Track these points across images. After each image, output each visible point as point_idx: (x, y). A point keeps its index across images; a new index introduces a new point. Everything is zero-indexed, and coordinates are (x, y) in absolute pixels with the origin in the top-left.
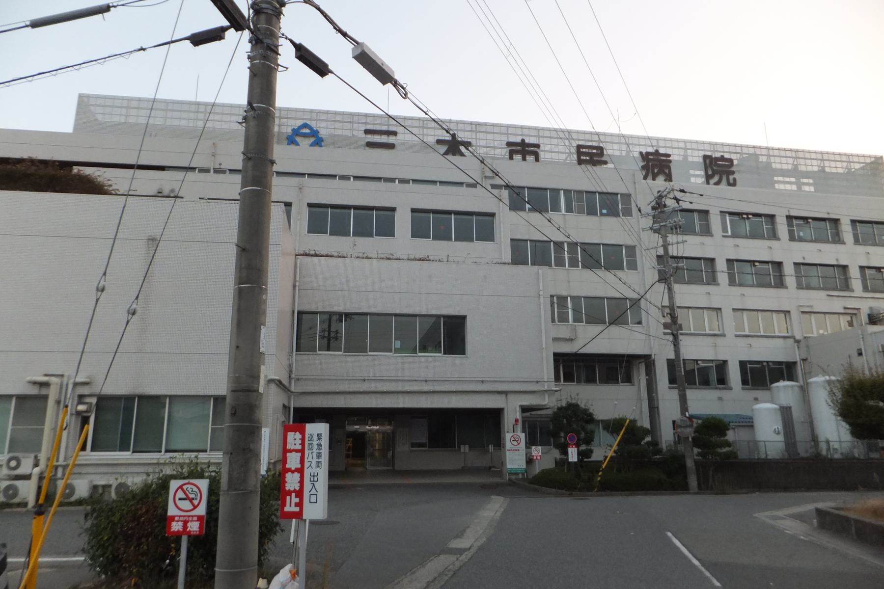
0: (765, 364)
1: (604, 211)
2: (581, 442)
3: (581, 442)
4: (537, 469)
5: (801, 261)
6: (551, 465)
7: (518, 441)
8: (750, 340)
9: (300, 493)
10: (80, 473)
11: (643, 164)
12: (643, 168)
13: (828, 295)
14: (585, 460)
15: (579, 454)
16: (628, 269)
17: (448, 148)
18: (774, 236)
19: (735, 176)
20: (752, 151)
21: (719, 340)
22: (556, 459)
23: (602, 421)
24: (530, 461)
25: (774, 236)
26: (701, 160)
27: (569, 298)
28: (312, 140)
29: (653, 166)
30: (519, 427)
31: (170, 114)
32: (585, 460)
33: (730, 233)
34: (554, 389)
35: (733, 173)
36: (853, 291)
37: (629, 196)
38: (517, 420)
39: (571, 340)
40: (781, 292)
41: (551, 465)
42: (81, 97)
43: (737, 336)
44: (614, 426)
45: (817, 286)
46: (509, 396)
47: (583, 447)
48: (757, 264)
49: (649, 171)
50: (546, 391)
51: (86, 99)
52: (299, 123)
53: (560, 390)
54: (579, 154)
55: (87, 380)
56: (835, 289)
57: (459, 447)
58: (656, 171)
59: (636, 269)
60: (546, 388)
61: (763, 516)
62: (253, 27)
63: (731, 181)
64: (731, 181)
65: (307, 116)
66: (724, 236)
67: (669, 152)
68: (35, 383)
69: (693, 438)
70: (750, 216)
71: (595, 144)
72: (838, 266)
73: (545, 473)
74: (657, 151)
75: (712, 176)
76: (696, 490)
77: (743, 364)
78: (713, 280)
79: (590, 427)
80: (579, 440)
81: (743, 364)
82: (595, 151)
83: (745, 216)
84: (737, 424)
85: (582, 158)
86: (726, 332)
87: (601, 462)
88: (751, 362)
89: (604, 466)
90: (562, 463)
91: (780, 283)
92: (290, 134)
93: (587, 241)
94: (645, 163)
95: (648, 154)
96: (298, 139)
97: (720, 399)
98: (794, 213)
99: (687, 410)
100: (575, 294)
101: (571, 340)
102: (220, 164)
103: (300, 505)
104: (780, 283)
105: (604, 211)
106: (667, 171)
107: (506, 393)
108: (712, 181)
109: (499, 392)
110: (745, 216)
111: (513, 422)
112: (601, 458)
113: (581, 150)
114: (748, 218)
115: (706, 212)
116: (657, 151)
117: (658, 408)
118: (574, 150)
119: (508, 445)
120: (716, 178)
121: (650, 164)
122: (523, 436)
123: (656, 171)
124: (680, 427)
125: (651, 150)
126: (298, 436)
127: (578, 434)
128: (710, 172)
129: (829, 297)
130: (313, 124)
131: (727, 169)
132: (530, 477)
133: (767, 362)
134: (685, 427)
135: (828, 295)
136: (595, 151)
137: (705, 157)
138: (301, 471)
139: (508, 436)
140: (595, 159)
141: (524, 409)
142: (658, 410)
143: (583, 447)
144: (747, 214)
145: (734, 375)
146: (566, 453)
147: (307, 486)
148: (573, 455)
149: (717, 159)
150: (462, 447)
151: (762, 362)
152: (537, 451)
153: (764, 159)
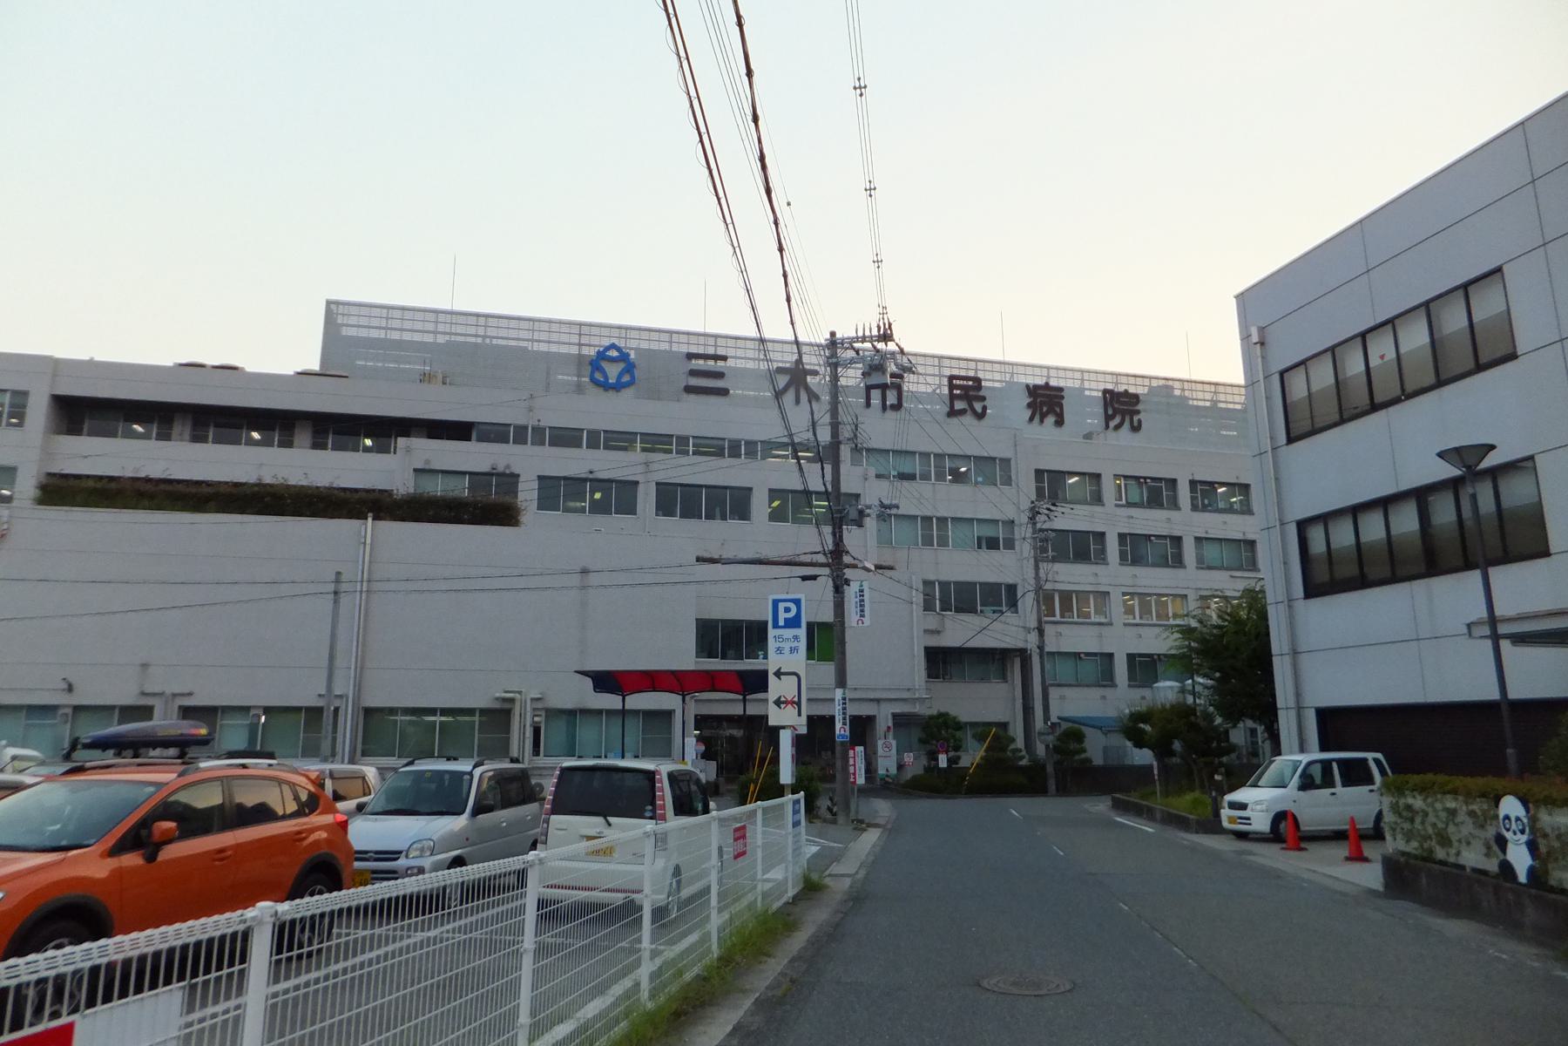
0: (1156, 657)
1: (980, 479)
2: (950, 749)
3: (950, 749)
4: (909, 774)
5: (1204, 535)
6: (921, 772)
7: (888, 747)
8: (1141, 630)
9: (854, 774)
10: (540, 775)
11: (1029, 400)
12: (1029, 406)
13: (1232, 577)
14: (954, 766)
15: (949, 760)
16: (1004, 549)
17: (790, 380)
18: (1174, 505)
19: (1141, 416)
20: (1162, 383)
21: (1105, 630)
22: (924, 766)
23: (974, 725)
24: (900, 767)
25: (1174, 505)
26: (1100, 394)
27: (937, 583)
28: (622, 365)
29: (1042, 404)
30: (891, 735)
31: (430, 327)
32: (954, 766)
33: (1124, 502)
34: (924, 696)
35: (1138, 412)
36: (1259, 571)
37: (1008, 461)
38: (889, 728)
39: (938, 632)
40: (1180, 572)
41: (921, 772)
42: (329, 303)
43: (1125, 625)
44: (981, 730)
45: (1218, 563)
46: (881, 703)
47: (952, 754)
48: (1152, 538)
49: (1036, 410)
50: (917, 699)
51: (333, 307)
52: (606, 342)
53: (931, 698)
54: (952, 387)
55: (539, 696)
56: (1240, 568)
57: (820, 753)
58: (1045, 409)
59: (1014, 549)
60: (917, 696)
61: (1086, 806)
62: (1011, 813)
63: (1136, 424)
64: (1136, 424)
65: (616, 333)
66: (1117, 506)
67: (1062, 384)
68: (497, 699)
69: (1054, 746)
70: (1148, 481)
71: (971, 374)
72: (1102, 654)
73: (915, 778)
74: (1047, 384)
75: (1111, 417)
76: (1054, 792)
77: (1131, 658)
78: (1101, 558)
79: (958, 734)
80: (948, 746)
81: (1131, 658)
82: (970, 383)
83: (1142, 480)
84: (1110, 729)
85: (955, 392)
86: (1113, 621)
87: (969, 768)
88: (1141, 655)
89: (971, 771)
90: (932, 769)
91: (1178, 562)
92: (594, 358)
93: (959, 516)
94: (1032, 399)
95: (1036, 387)
96: (604, 364)
97: (1104, 698)
98: (1197, 478)
99: (1049, 719)
100: (943, 578)
101: (938, 632)
102: (539, 421)
103: (855, 778)
104: (1178, 562)
105: (980, 479)
106: (1058, 410)
107: (878, 701)
108: (1112, 424)
109: (871, 700)
110: (1142, 480)
111: (886, 728)
112: (969, 765)
113: (954, 381)
114: (1146, 483)
115: (1099, 476)
116: (1047, 384)
117: (1033, 708)
118: (945, 381)
119: (880, 751)
120: (1117, 420)
121: (1038, 400)
122: (894, 743)
123: (1045, 409)
124: (1043, 734)
125: (1040, 381)
126: (852, 751)
127: (947, 740)
128: (1110, 412)
129: (1233, 579)
130: (621, 344)
131: (1131, 408)
132: (902, 782)
133: (1159, 655)
134: (1048, 734)
135: (1232, 577)
136: (970, 383)
137: (1105, 392)
138: (854, 765)
139: (880, 743)
140: (971, 393)
141: (895, 716)
142: (1033, 711)
143: (952, 754)
144: (1145, 478)
145: (1121, 669)
146: (937, 760)
147: (857, 772)
148: (943, 761)
149: (1120, 394)
150: (823, 753)
151: (1153, 655)
152: (909, 758)
153: (1177, 393)
